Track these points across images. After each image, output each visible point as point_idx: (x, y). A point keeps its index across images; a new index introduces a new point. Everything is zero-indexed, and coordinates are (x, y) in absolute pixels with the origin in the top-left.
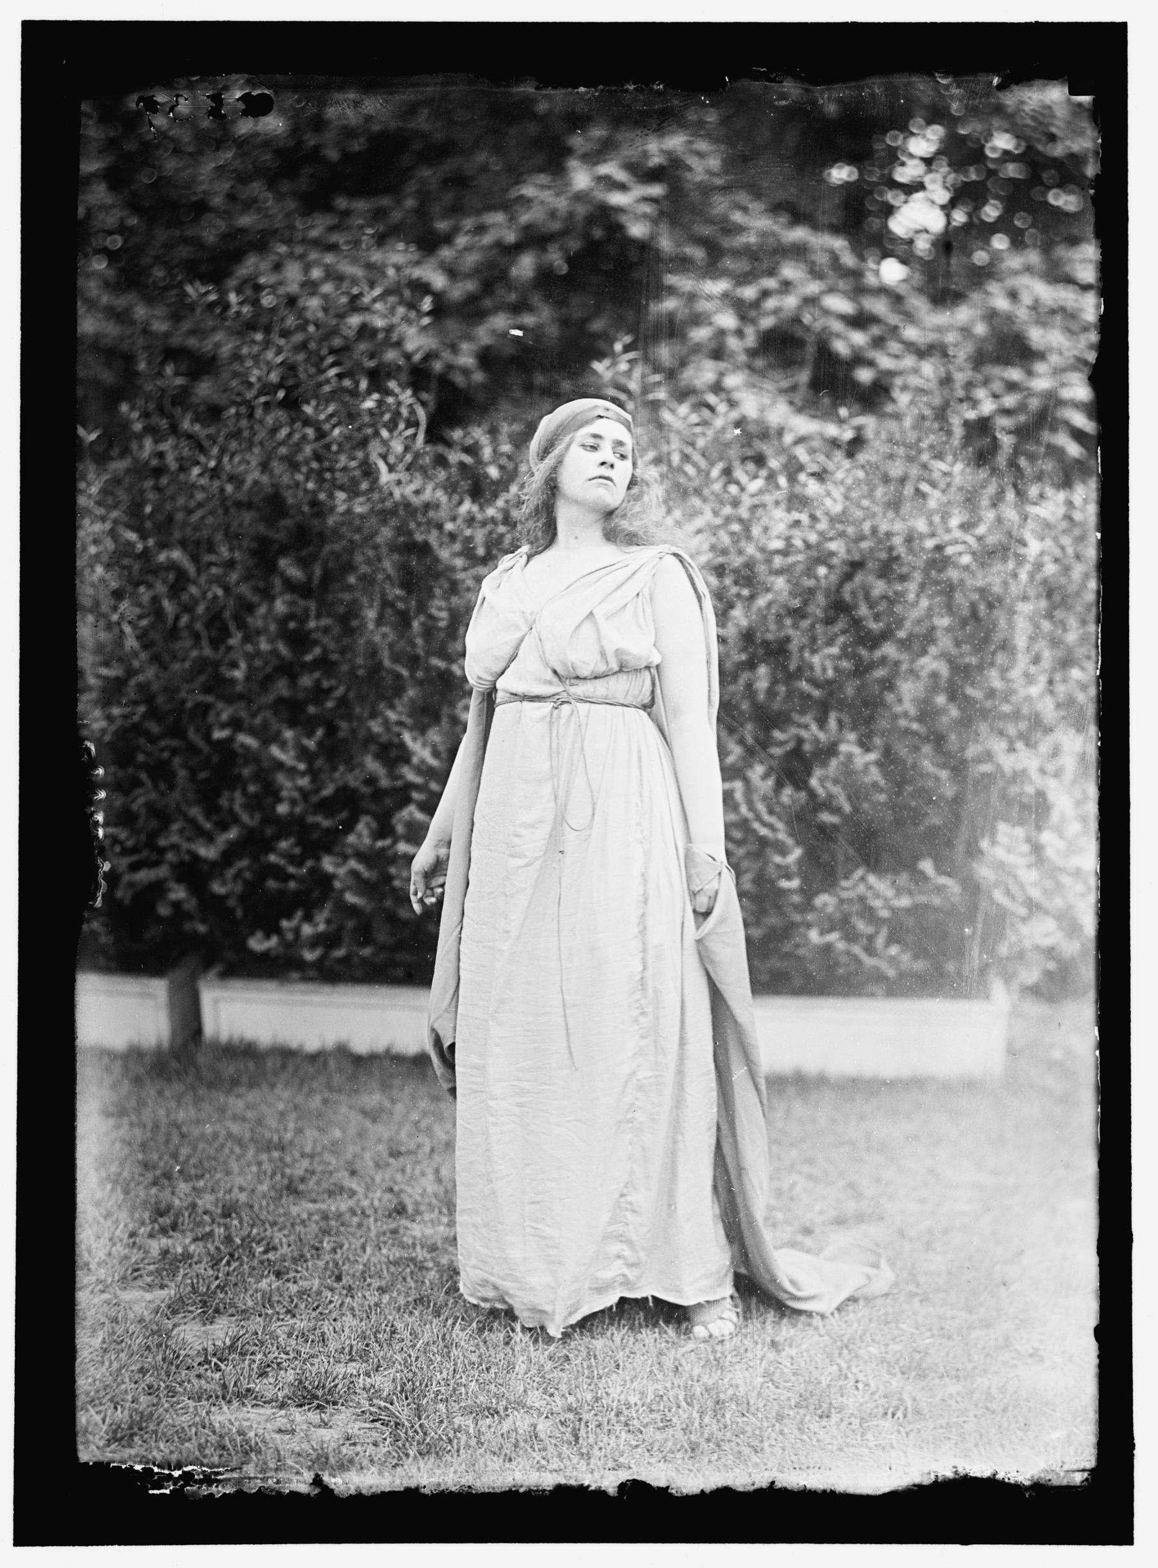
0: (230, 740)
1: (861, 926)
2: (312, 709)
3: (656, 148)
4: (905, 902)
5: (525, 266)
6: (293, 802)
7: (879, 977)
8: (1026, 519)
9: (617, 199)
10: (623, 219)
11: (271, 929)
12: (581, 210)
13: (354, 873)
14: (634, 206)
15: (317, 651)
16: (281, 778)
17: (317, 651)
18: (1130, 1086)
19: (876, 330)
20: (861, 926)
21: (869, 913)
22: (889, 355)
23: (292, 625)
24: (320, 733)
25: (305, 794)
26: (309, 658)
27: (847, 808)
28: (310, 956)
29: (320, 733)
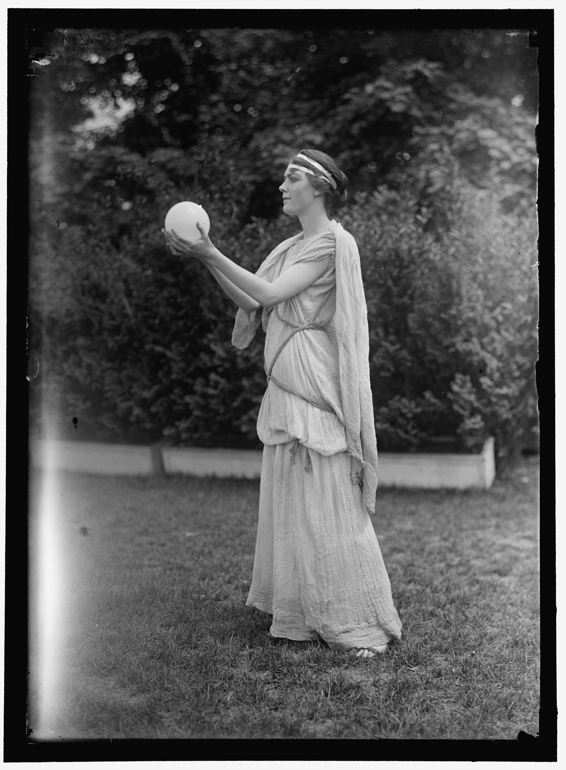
0: (152, 350)
1: (400, 420)
2: (185, 335)
3: (412, 67)
4: (418, 410)
5: (355, 129)
6: (178, 374)
7: (410, 444)
8: (99, 246)
9: (385, 95)
10: (389, 104)
11: (172, 425)
12: (371, 102)
13: (197, 403)
14: (398, 98)
15: (184, 311)
16: (172, 364)
17: (184, 311)
18: (7, 412)
19: (516, 143)
20: (400, 420)
21: (403, 415)
22: (518, 154)
23: (172, 301)
24: (188, 345)
25: (183, 370)
26: (180, 314)
27: (392, 369)
28: (184, 436)
29: (188, 345)
